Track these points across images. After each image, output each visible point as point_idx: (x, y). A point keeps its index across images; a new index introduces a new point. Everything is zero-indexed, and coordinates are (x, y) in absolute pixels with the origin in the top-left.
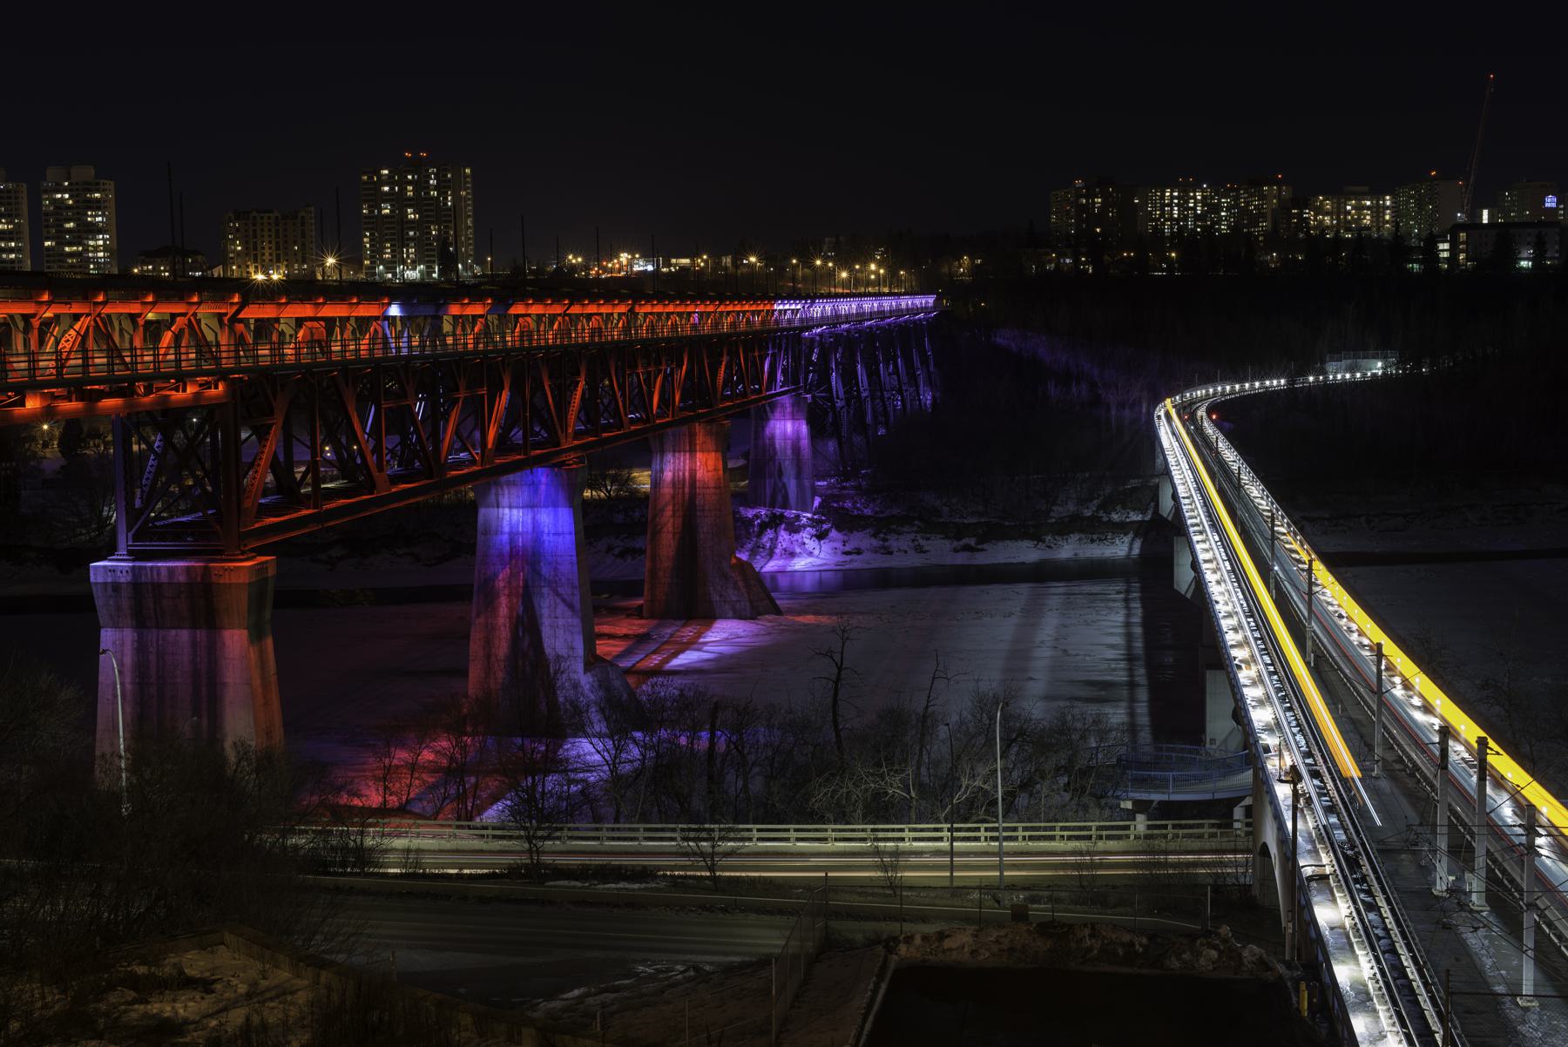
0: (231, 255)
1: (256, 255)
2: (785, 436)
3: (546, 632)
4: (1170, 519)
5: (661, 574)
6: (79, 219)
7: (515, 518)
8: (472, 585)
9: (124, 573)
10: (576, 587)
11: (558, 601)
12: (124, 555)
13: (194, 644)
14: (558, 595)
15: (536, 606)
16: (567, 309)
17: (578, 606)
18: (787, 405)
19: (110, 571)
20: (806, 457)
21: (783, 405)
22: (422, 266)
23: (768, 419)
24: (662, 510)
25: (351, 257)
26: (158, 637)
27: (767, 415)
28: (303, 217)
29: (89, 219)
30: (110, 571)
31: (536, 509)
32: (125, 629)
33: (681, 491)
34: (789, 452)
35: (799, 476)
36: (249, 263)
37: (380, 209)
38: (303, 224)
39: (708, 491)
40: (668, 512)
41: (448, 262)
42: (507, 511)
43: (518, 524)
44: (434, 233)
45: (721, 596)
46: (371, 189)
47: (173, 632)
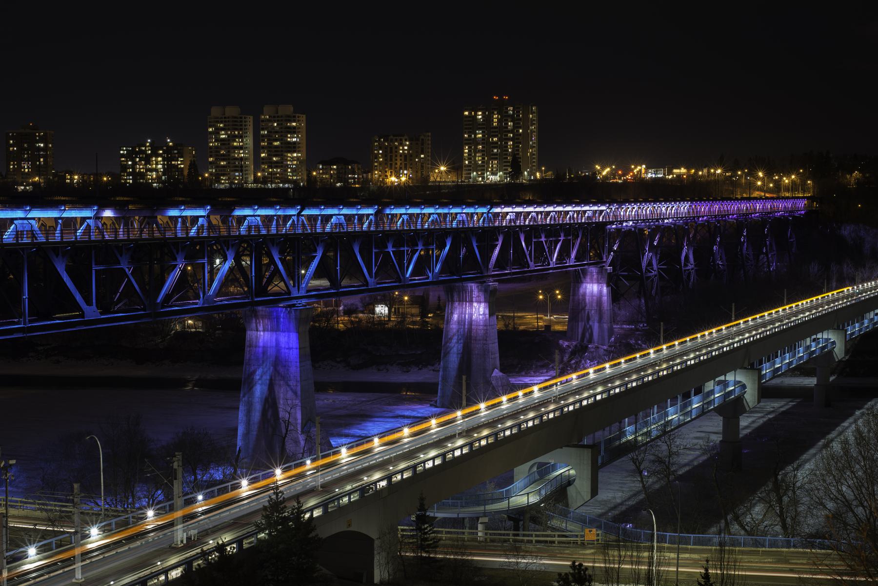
0: (376, 164)
1: (391, 165)
6: (282, 140)
11: (288, 389)
14: (289, 386)
15: (276, 392)
16: (490, 210)
17: (299, 393)
20: (606, 309)
21: (592, 273)
22: (501, 173)
23: (582, 282)
24: (451, 339)
25: (456, 167)
27: (581, 280)
28: (423, 140)
29: (289, 139)
31: (278, 333)
34: (594, 305)
35: (600, 321)
36: (387, 170)
37: (476, 134)
38: (422, 144)
40: (454, 341)
41: (516, 169)
44: (510, 150)
46: (470, 121)
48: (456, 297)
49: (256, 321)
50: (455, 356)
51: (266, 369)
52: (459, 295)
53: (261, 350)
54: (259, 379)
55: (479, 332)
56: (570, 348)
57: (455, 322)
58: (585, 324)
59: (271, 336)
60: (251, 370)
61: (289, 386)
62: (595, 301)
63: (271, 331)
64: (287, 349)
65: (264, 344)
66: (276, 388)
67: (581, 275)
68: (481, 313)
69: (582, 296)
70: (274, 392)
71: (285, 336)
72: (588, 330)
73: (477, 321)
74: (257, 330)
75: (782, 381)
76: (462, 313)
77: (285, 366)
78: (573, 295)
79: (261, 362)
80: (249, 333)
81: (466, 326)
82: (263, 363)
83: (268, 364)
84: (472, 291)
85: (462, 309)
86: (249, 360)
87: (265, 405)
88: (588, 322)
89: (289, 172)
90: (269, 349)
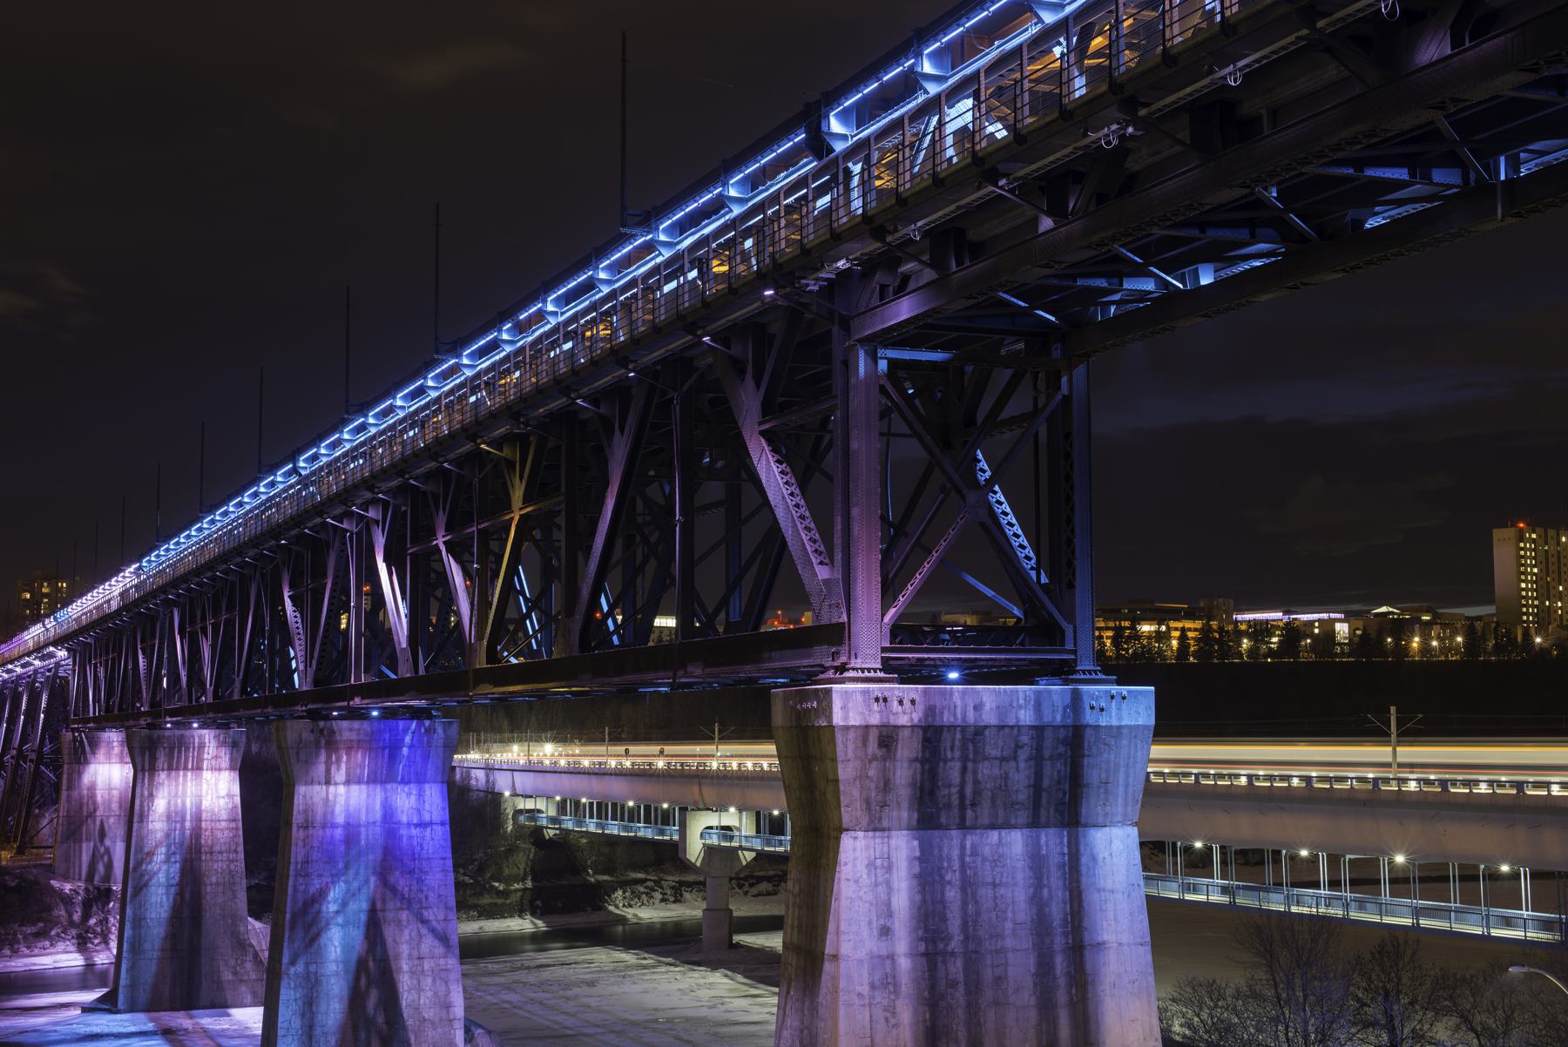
2: (110, 782)
3: (405, 982)
4: (698, 864)
5: (147, 946)
7: (353, 802)
8: (1398, 735)
9: (907, 703)
10: (451, 909)
11: (424, 931)
12: (875, 670)
13: (1037, 862)
14: (424, 922)
15: (389, 940)
18: (115, 744)
19: (877, 700)
21: (110, 743)
23: (87, 762)
24: (151, 854)
26: (963, 847)
30: (877, 700)
31: (389, 786)
32: (894, 833)
33: (178, 825)
39: (218, 825)
40: (160, 857)
42: (341, 789)
43: (359, 811)
45: (235, 973)
47: (994, 836)
48: (162, 760)
49: (329, 758)
50: (161, 891)
51: (355, 884)
52: (170, 756)
53: (339, 833)
54: (337, 912)
55: (219, 834)
56: (78, 893)
57: (161, 815)
58: (95, 846)
59: (368, 796)
60: (312, 890)
61: (424, 922)
62: (116, 799)
63: (368, 782)
64: (416, 826)
65: (348, 815)
66: (389, 932)
67: (87, 748)
68: (223, 792)
69: (88, 789)
70: (383, 944)
71: (409, 794)
72: (102, 857)
73: (212, 812)
74: (328, 782)
75: (481, 928)
76: (176, 795)
77: (411, 872)
78: (69, 788)
79: (341, 865)
80: (301, 790)
81: (188, 824)
82: (347, 867)
83: (362, 871)
84: (202, 746)
85: (177, 785)
86: (307, 862)
87: (357, 979)
88: (102, 840)
89: (592, 332)
90: (363, 830)
